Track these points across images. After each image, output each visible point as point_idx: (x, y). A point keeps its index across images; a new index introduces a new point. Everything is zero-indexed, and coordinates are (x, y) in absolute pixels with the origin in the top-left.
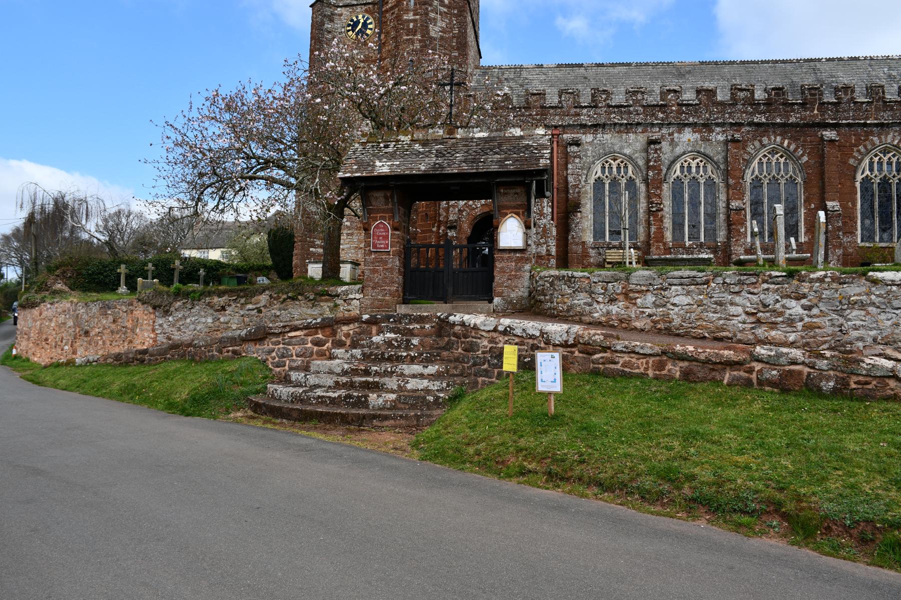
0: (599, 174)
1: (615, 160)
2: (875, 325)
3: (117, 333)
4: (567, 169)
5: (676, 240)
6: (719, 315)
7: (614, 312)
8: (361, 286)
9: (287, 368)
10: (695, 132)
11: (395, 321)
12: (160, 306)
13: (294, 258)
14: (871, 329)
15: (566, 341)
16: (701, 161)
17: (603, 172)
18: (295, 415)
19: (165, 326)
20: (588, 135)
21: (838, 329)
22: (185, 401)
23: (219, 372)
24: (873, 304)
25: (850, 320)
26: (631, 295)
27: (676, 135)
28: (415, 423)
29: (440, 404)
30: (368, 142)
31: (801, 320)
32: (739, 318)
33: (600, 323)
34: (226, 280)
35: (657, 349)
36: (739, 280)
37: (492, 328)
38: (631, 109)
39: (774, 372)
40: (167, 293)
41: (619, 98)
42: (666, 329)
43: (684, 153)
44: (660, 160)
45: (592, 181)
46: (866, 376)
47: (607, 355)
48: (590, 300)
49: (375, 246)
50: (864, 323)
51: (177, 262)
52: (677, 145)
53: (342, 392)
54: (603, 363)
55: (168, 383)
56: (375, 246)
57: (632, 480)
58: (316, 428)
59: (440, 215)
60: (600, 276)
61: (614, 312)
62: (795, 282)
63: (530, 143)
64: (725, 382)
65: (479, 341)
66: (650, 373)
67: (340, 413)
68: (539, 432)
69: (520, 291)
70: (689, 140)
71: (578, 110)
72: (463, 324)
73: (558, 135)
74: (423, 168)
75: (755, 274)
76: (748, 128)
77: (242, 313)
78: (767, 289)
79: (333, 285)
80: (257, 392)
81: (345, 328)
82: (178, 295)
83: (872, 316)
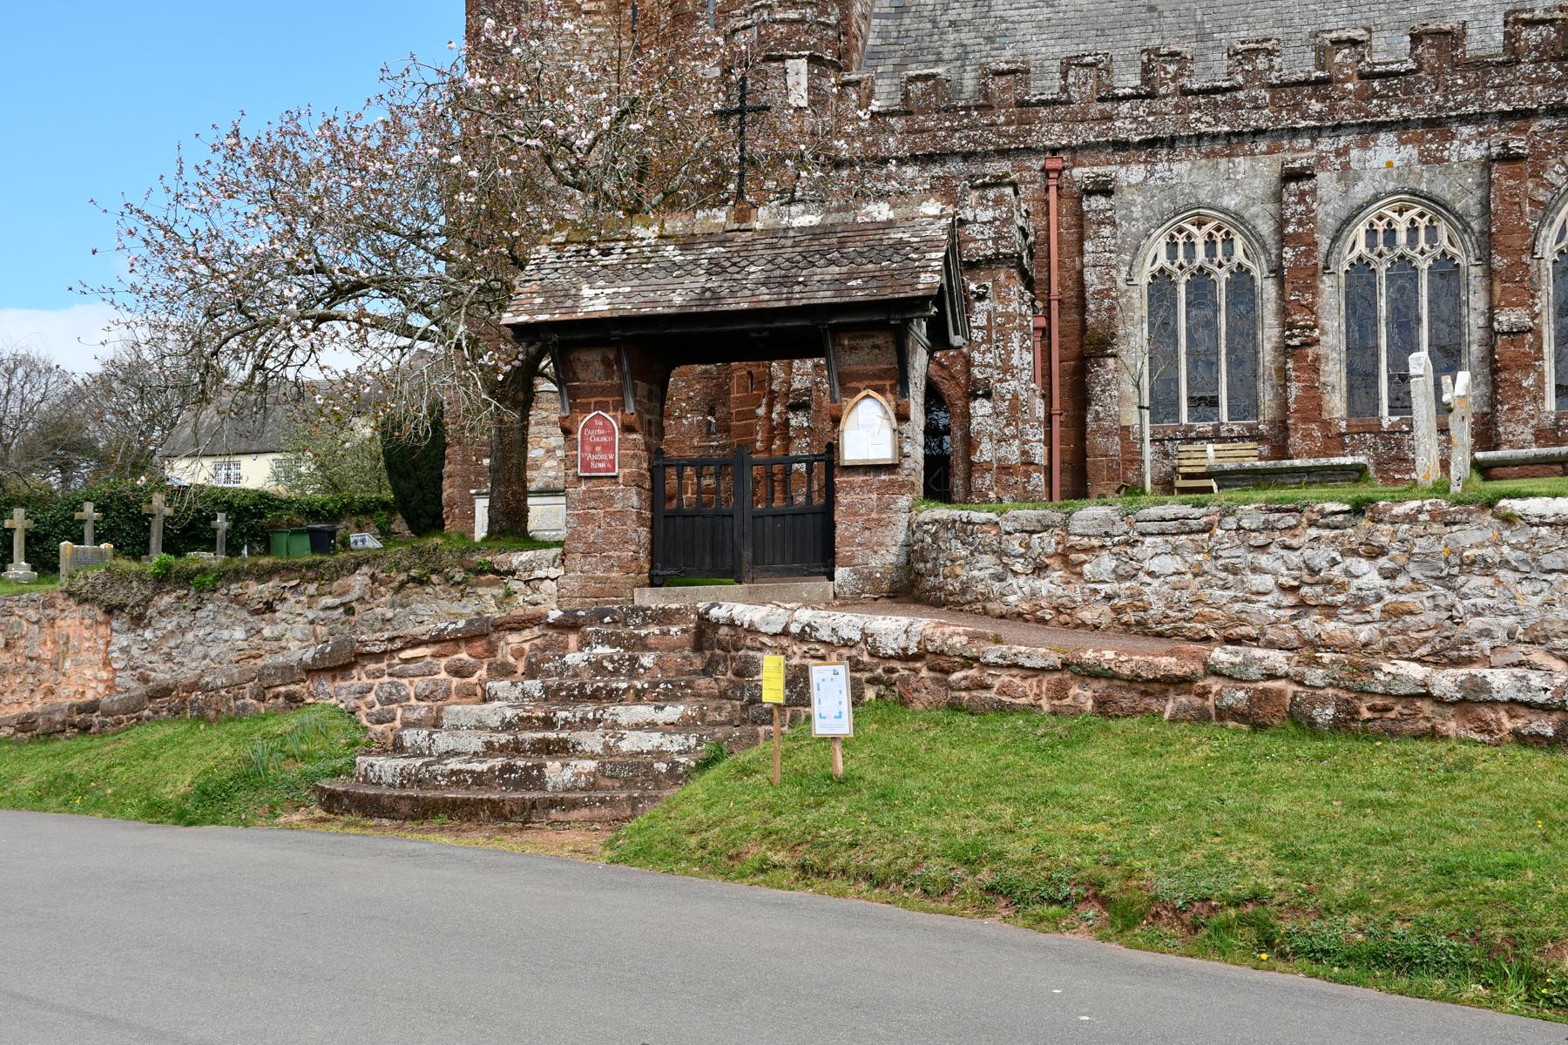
0: (1163, 261)
1: (1200, 225)
2: (1511, 606)
3: (15, 674)
4: (1081, 253)
5: (1358, 415)
6: (1231, 593)
7: (1044, 593)
8: (559, 550)
9: (398, 723)
10: (1402, 142)
11: (614, 622)
12: (121, 607)
13: (446, 483)
14: (1504, 614)
15: (905, 649)
16: (1422, 215)
17: (1172, 256)
18: (405, 808)
19: (135, 651)
20: (1134, 167)
21: (1446, 615)
22: (185, 798)
23: (257, 736)
24: (1505, 563)
25: (1465, 596)
26: (1073, 556)
27: (1355, 153)
28: (629, 812)
29: (680, 776)
30: (568, 242)
31: (1379, 598)
32: (1268, 598)
33: (1020, 615)
34: (281, 540)
35: (1055, 659)
36: (1266, 521)
37: (779, 629)
38: (1241, 95)
39: (1241, 694)
40: (139, 576)
41: (1214, 69)
42: (1138, 623)
43: (1376, 198)
44: (1312, 220)
45: (1143, 279)
46: (1386, 695)
47: (973, 673)
48: (1000, 569)
49: (586, 466)
50: (1491, 602)
51: (158, 499)
52: (1358, 178)
53: (498, 762)
54: (967, 689)
55: (147, 767)
56: (586, 466)
57: (916, 865)
58: (442, 829)
59: (771, 379)
60: (1016, 519)
61: (1044, 593)
62: (1365, 523)
63: (906, 236)
64: (1166, 716)
65: (759, 654)
66: (1044, 702)
67: (489, 800)
68: (809, 806)
69: (886, 557)
70: (1389, 164)
71: (1108, 106)
72: (731, 623)
73: (1060, 171)
74: (678, 300)
75: (1295, 510)
76: (1547, 122)
77: (311, 615)
78: (1317, 539)
79: (500, 552)
80: (336, 773)
81: (514, 638)
82: (163, 579)
83: (1506, 588)
